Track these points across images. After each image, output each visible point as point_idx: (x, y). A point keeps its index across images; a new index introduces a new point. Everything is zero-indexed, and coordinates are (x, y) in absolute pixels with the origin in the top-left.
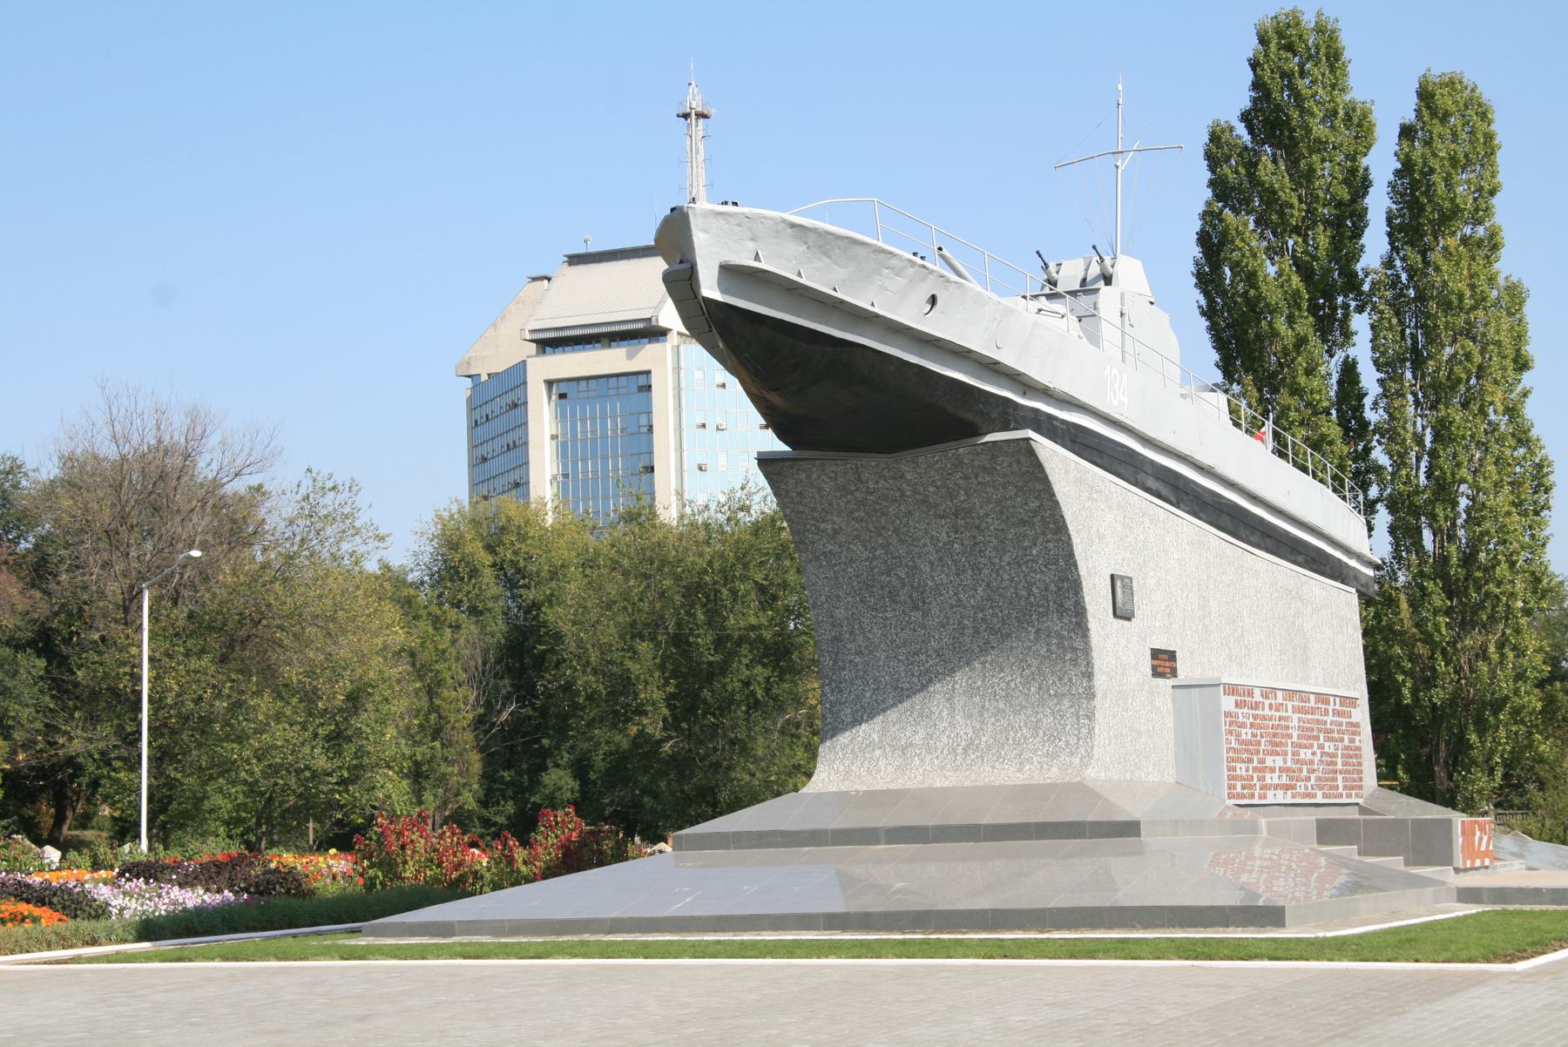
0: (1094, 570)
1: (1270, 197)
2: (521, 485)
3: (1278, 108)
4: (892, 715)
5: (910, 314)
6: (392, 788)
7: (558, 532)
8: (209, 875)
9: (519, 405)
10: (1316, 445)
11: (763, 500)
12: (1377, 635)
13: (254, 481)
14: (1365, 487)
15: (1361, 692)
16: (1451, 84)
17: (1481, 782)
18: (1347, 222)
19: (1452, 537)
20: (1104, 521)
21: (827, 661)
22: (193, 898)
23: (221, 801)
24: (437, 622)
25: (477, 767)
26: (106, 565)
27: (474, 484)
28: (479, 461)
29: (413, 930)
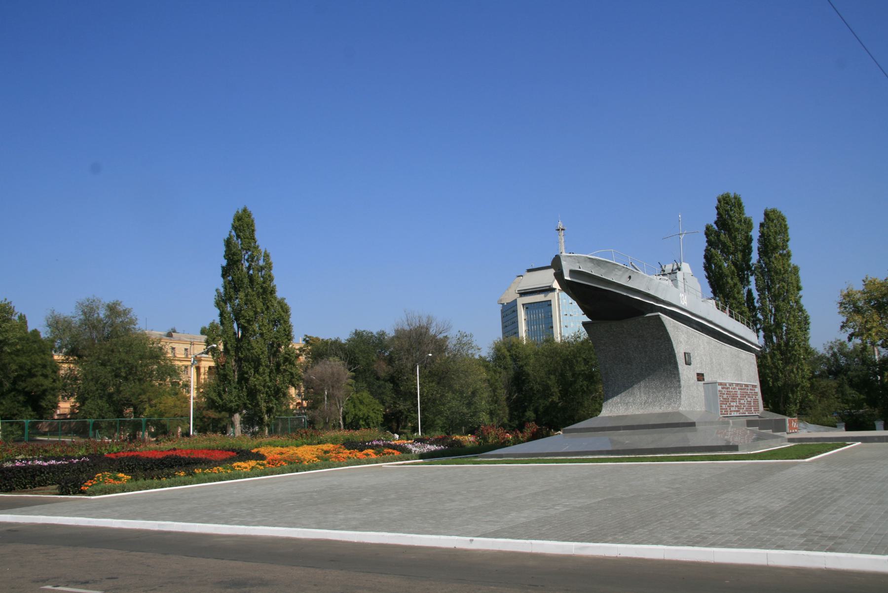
0: (680, 351)
1: (724, 244)
2: (516, 333)
3: (725, 220)
4: (623, 394)
5: (623, 281)
6: (484, 417)
7: (527, 345)
8: (436, 442)
9: (515, 311)
10: (741, 313)
11: (584, 335)
12: (761, 367)
13: (445, 335)
14: (756, 325)
15: (757, 383)
16: (774, 211)
17: (793, 408)
18: (747, 250)
19: (782, 338)
20: (682, 338)
21: (604, 380)
22: (433, 448)
23: (440, 421)
24: (495, 371)
25: (507, 411)
26: (407, 359)
27: (504, 333)
28: (504, 327)
29: (492, 456)
